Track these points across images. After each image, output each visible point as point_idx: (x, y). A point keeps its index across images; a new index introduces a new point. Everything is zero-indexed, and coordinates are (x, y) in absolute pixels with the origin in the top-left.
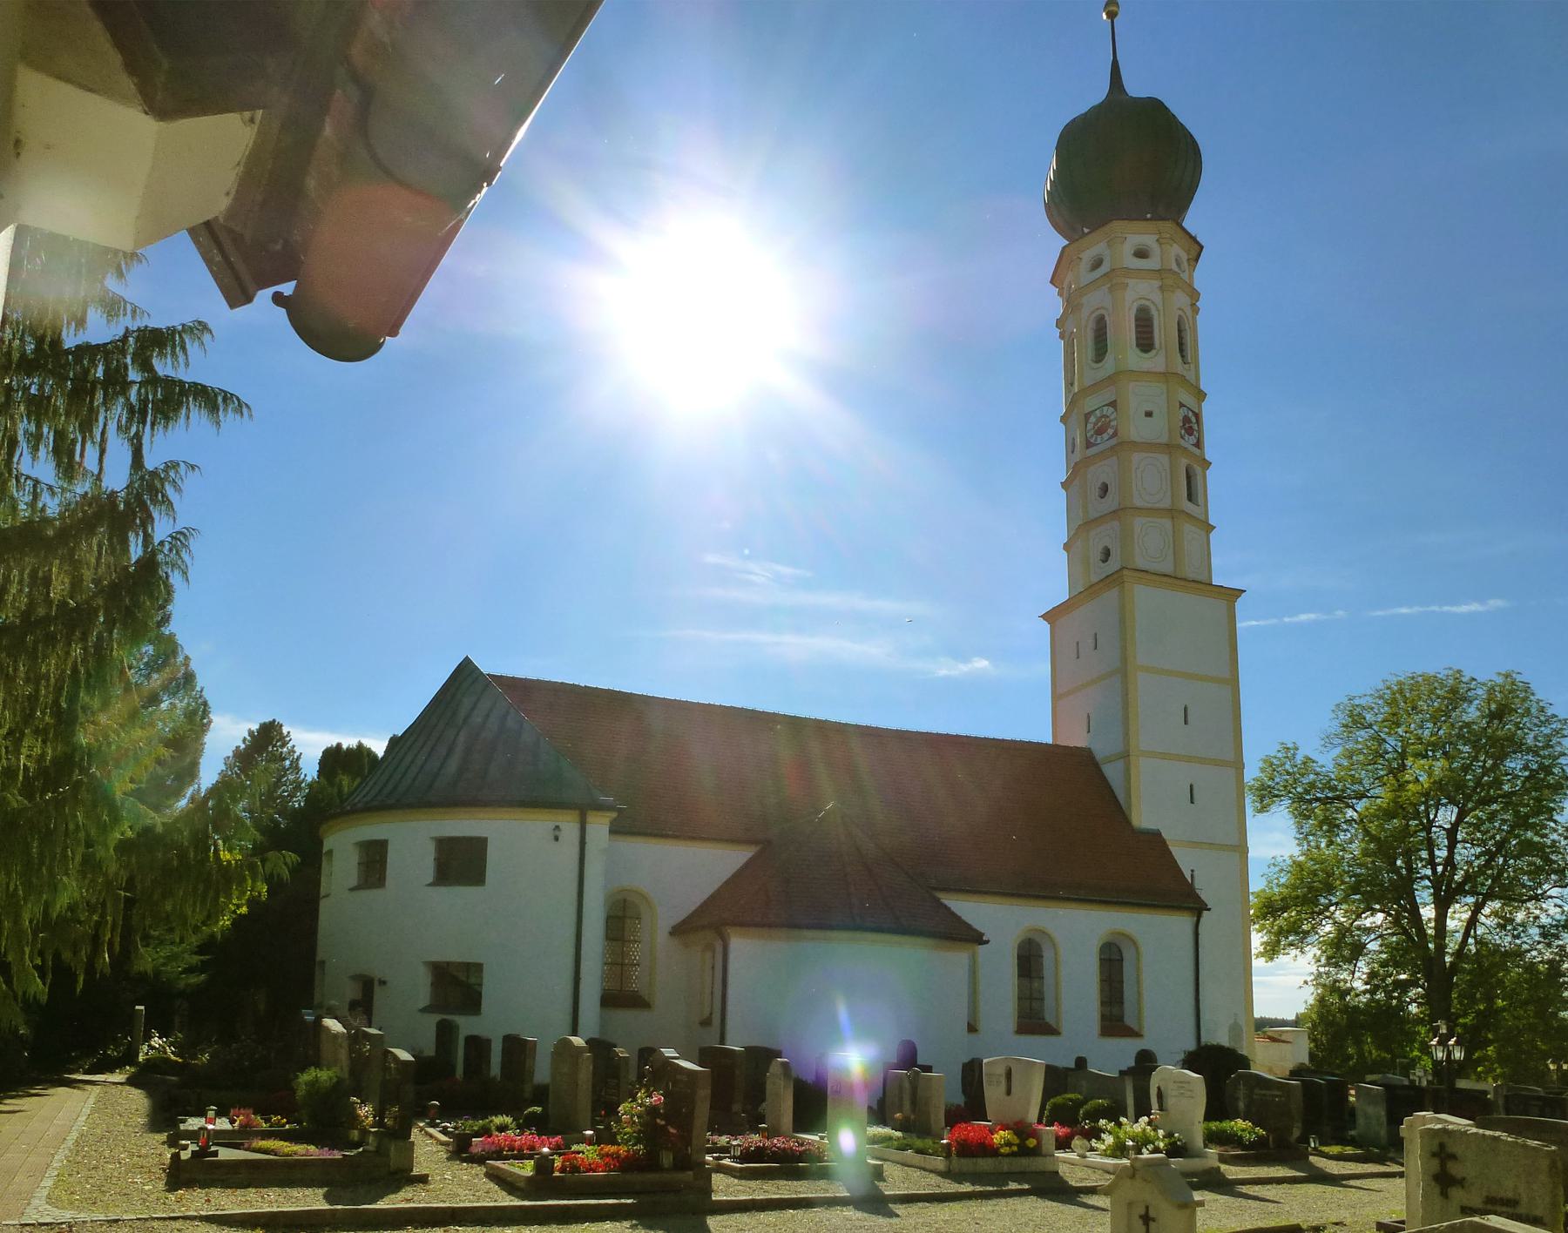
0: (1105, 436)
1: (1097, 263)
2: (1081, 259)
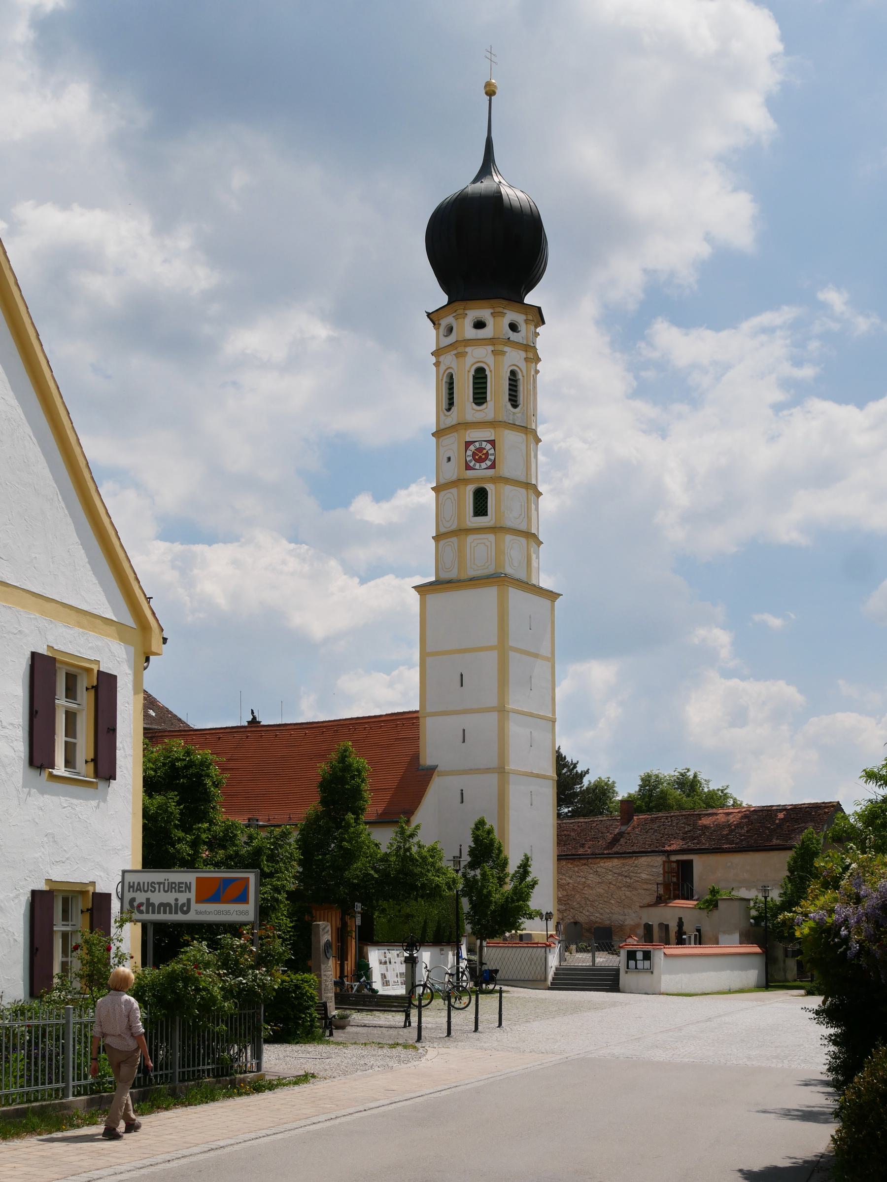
0: (484, 465)
1: (480, 325)
2: (466, 314)
